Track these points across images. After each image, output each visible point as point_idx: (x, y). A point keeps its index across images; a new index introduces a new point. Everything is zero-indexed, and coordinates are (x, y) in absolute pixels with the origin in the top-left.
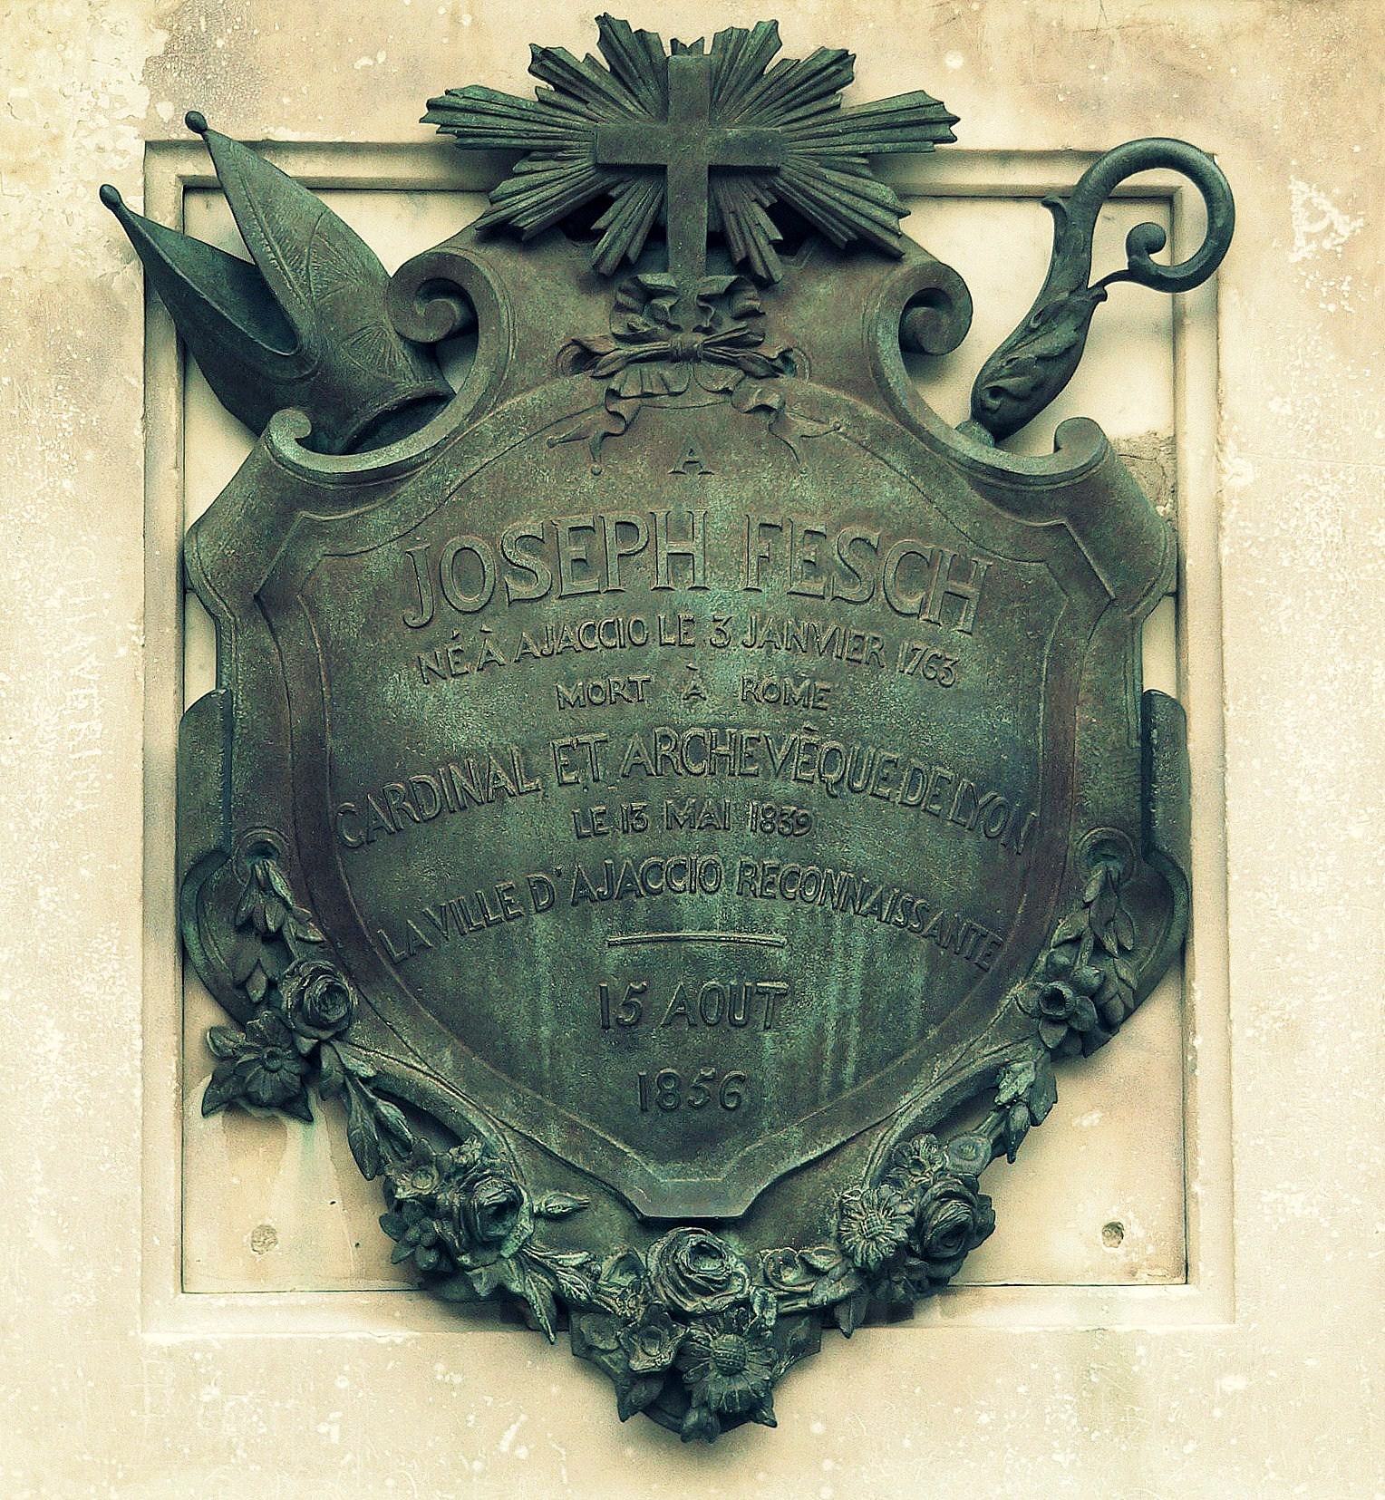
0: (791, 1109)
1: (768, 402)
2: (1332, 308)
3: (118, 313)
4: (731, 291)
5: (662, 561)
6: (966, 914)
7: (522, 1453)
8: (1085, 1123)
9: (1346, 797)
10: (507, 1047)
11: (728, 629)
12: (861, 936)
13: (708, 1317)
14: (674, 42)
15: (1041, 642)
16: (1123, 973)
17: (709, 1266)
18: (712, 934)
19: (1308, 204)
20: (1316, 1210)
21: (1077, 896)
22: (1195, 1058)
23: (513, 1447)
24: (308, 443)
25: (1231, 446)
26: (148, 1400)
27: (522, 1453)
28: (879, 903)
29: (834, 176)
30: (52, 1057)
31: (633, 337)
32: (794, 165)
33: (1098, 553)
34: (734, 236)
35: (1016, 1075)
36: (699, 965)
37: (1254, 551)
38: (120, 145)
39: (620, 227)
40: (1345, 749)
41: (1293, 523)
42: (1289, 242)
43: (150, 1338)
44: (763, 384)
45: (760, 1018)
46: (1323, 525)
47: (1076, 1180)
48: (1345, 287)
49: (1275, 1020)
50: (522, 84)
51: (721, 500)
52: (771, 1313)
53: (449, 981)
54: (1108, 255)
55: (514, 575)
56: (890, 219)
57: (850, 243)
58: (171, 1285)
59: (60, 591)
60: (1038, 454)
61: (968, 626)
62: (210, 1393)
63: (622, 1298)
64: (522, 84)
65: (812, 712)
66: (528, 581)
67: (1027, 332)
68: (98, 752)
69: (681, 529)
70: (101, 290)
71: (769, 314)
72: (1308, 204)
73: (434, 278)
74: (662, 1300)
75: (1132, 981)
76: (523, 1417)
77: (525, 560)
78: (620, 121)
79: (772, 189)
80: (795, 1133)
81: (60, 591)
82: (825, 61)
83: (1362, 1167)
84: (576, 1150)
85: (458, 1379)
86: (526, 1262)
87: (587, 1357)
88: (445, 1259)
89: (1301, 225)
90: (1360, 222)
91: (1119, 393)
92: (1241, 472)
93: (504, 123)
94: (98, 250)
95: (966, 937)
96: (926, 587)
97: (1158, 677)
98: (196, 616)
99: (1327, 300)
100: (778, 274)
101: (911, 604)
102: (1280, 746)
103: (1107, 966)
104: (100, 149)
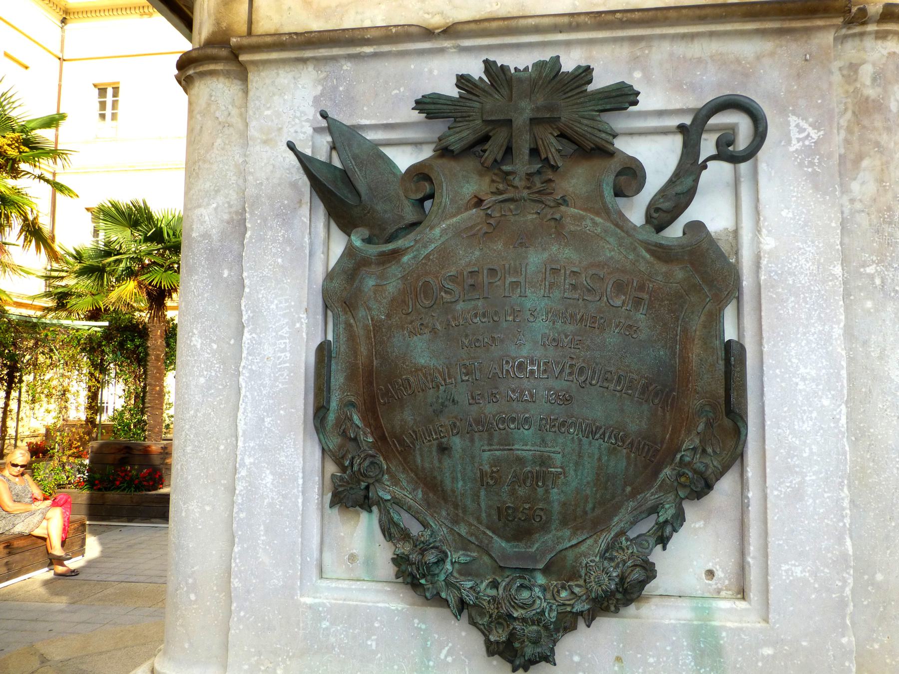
0: (564, 522)
1: (555, 217)
2: (810, 170)
3: (301, 194)
4: (539, 172)
5: (507, 285)
6: (643, 438)
7: (449, 659)
8: (697, 526)
9: (821, 387)
10: (443, 490)
11: (535, 313)
12: (595, 447)
13: (524, 620)
14: (516, 69)
15: (677, 319)
16: (715, 463)
17: (525, 594)
18: (528, 448)
19: (797, 126)
20: (807, 574)
21: (689, 423)
22: (749, 502)
23: (446, 657)
24: (368, 241)
25: (764, 231)
26: (301, 625)
27: (449, 659)
28: (604, 434)
29: (585, 122)
30: (268, 485)
31: (499, 192)
32: (566, 115)
33: (709, 274)
34: (542, 149)
35: (666, 510)
36: (521, 461)
37: (776, 277)
38: (304, 130)
39: (493, 150)
40: (820, 365)
41: (794, 264)
42: (789, 142)
43: (303, 600)
44: (554, 210)
45: (550, 483)
46: (808, 265)
47: (694, 554)
48: (816, 161)
49: (788, 487)
50: (453, 92)
51: (535, 259)
52: (554, 614)
53: (419, 461)
54: (708, 146)
55: (446, 292)
56: (611, 138)
57: (592, 149)
58: (314, 572)
59: (276, 302)
60: (675, 231)
61: (644, 312)
62: (325, 624)
63: (489, 602)
64: (453, 92)
65: (573, 350)
66: (450, 293)
67: (671, 182)
68: (288, 365)
69: (516, 272)
70: (294, 185)
71: (557, 181)
72: (797, 126)
73: (419, 173)
74: (503, 610)
75: (720, 467)
76: (450, 645)
77: (450, 286)
78: (493, 105)
79: (558, 128)
80: (567, 533)
81: (276, 302)
82: (580, 71)
83: (829, 555)
84: (472, 535)
85: (423, 627)
86: (449, 584)
87: (473, 623)
88: (415, 574)
89: (795, 134)
90: (822, 133)
91: (711, 210)
92: (768, 243)
93: (445, 107)
94: (294, 170)
95: (643, 448)
96: (625, 294)
97: (730, 334)
98: (330, 313)
99: (808, 167)
100: (560, 164)
101: (618, 302)
102: (789, 364)
103: (707, 460)
104: (296, 132)
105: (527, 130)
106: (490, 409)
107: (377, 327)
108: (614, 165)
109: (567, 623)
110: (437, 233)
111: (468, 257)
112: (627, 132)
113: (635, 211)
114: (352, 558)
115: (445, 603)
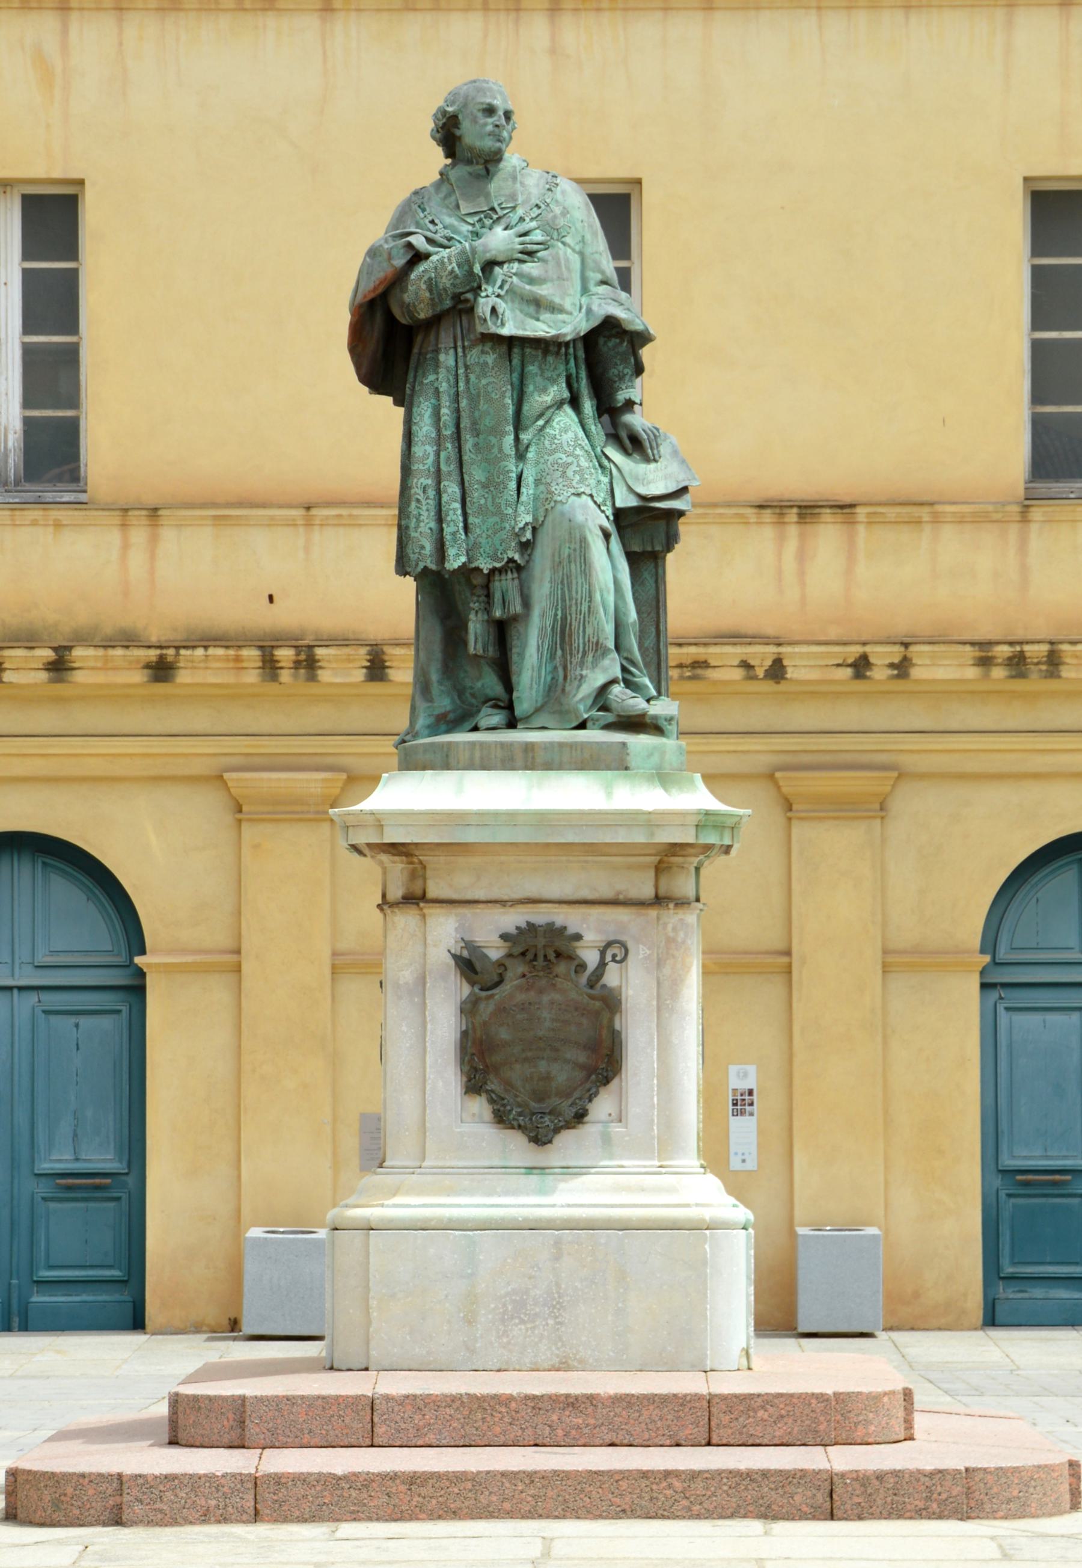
33: (611, 1003)
39: (530, 956)
51: (545, 999)
67: (597, 968)
73: (500, 964)
88: (501, 1118)
89: (641, 952)
92: (630, 992)
105: (543, 950)
106: (529, 1054)
107: (485, 1024)
108: (576, 963)
109: (557, 1130)
110: (507, 987)
111: (521, 997)
112: (419, 1225)
113: (584, 979)
114: (474, 1115)
115: (513, 1128)
